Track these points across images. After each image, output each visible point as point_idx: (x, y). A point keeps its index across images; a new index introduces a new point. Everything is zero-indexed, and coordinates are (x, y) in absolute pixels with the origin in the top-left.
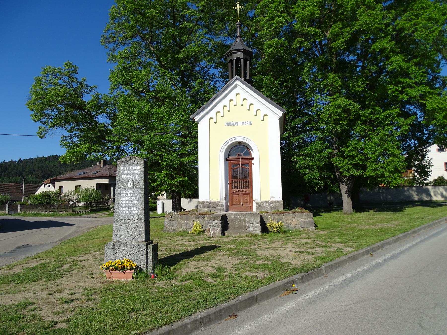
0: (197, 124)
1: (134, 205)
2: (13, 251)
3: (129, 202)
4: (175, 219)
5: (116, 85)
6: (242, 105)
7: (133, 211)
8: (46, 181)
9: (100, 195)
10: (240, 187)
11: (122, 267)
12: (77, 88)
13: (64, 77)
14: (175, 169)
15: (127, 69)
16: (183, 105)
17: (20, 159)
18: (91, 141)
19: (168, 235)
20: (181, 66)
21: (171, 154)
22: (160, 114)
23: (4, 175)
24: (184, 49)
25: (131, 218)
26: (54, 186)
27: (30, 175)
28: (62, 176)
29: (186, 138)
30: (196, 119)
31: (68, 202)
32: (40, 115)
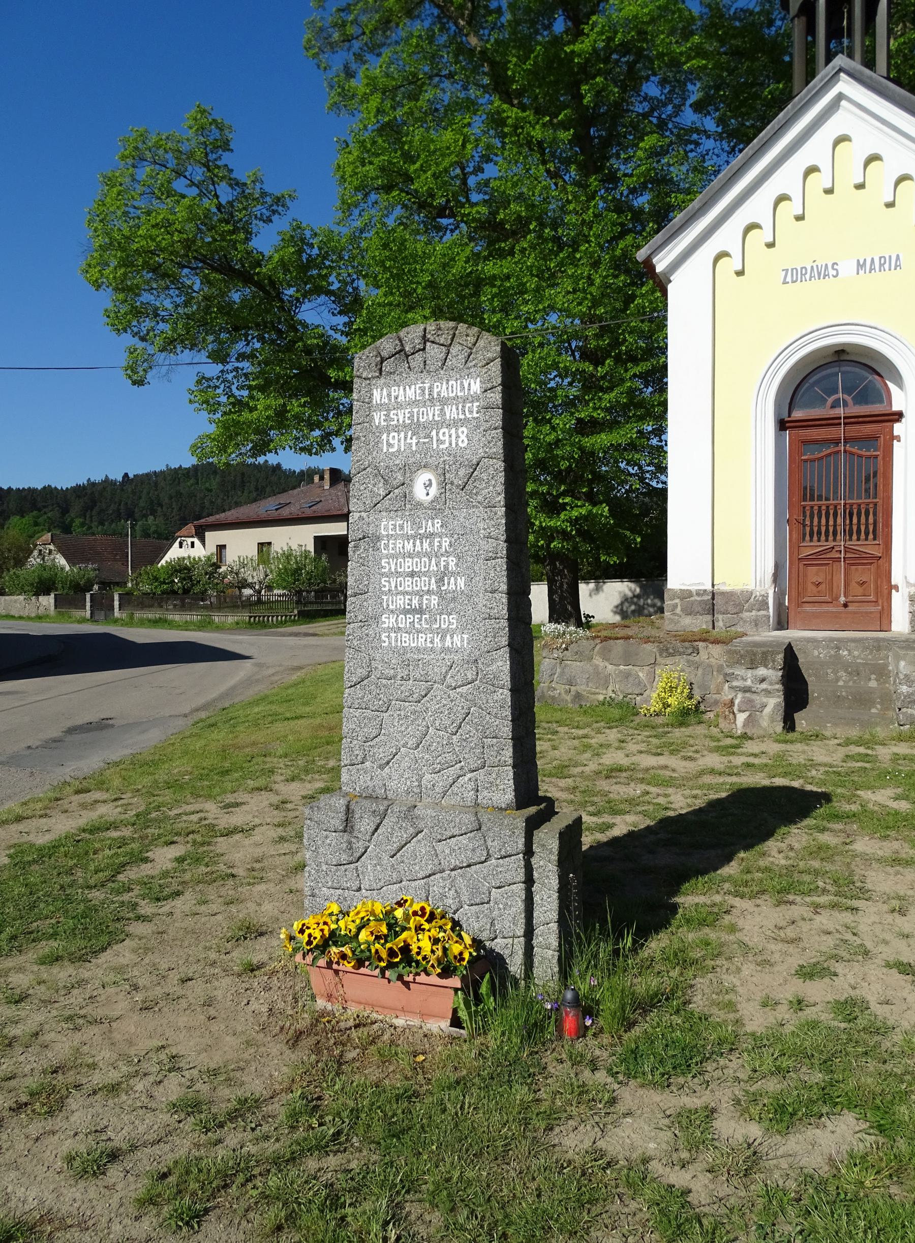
0: (661, 285)
1: (449, 601)
2: (55, 741)
3: (421, 584)
4: (580, 656)
5: (357, 189)
6: (860, 186)
7: (443, 634)
8: (184, 531)
9: (325, 569)
11: (392, 953)
12: (231, 203)
13: (190, 168)
14: (560, 477)
15: (392, 131)
16: (589, 242)
17: (126, 475)
18: (287, 389)
19: (558, 715)
20: (584, 88)
21: (549, 421)
22: (508, 277)
23: (91, 517)
24: (594, 18)
25: (436, 672)
26: (203, 541)
27: (152, 517)
28: (221, 517)
29: (603, 364)
30: (661, 264)
31: (240, 588)
32: (130, 316)
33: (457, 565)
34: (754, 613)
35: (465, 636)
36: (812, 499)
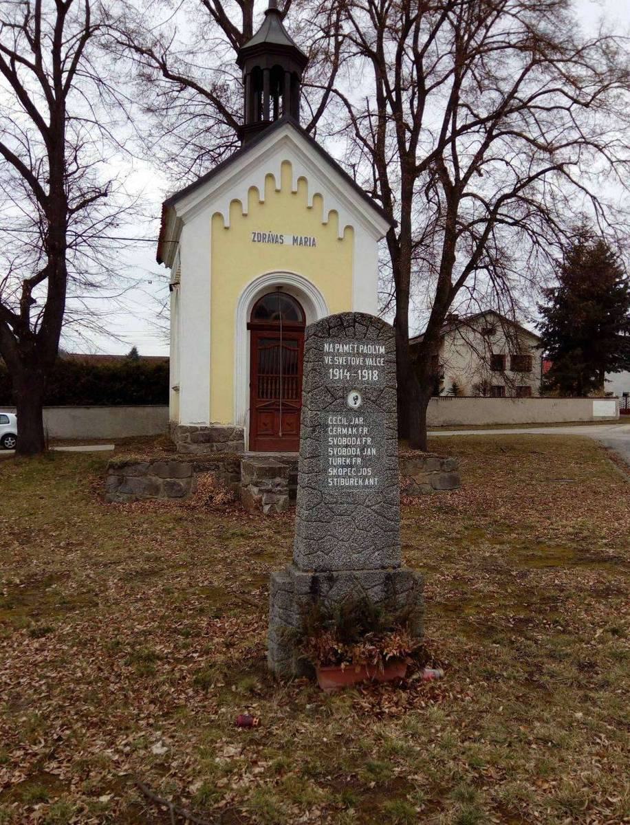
1: (367, 462)
3: (352, 451)
7: (364, 478)
10: (267, 394)
33: (372, 442)
34: (235, 442)
35: (376, 479)
36: (263, 373)
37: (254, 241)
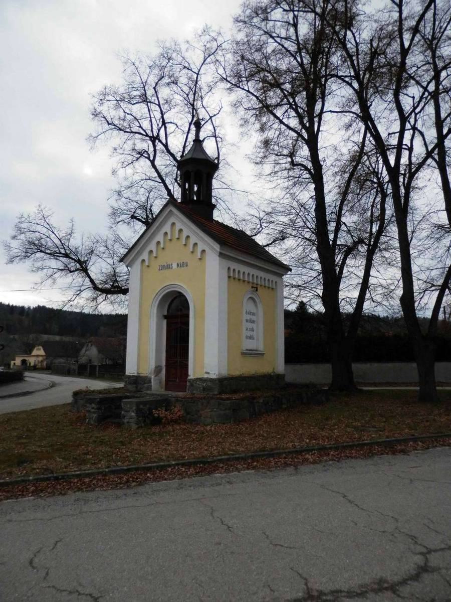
37: (159, 270)
